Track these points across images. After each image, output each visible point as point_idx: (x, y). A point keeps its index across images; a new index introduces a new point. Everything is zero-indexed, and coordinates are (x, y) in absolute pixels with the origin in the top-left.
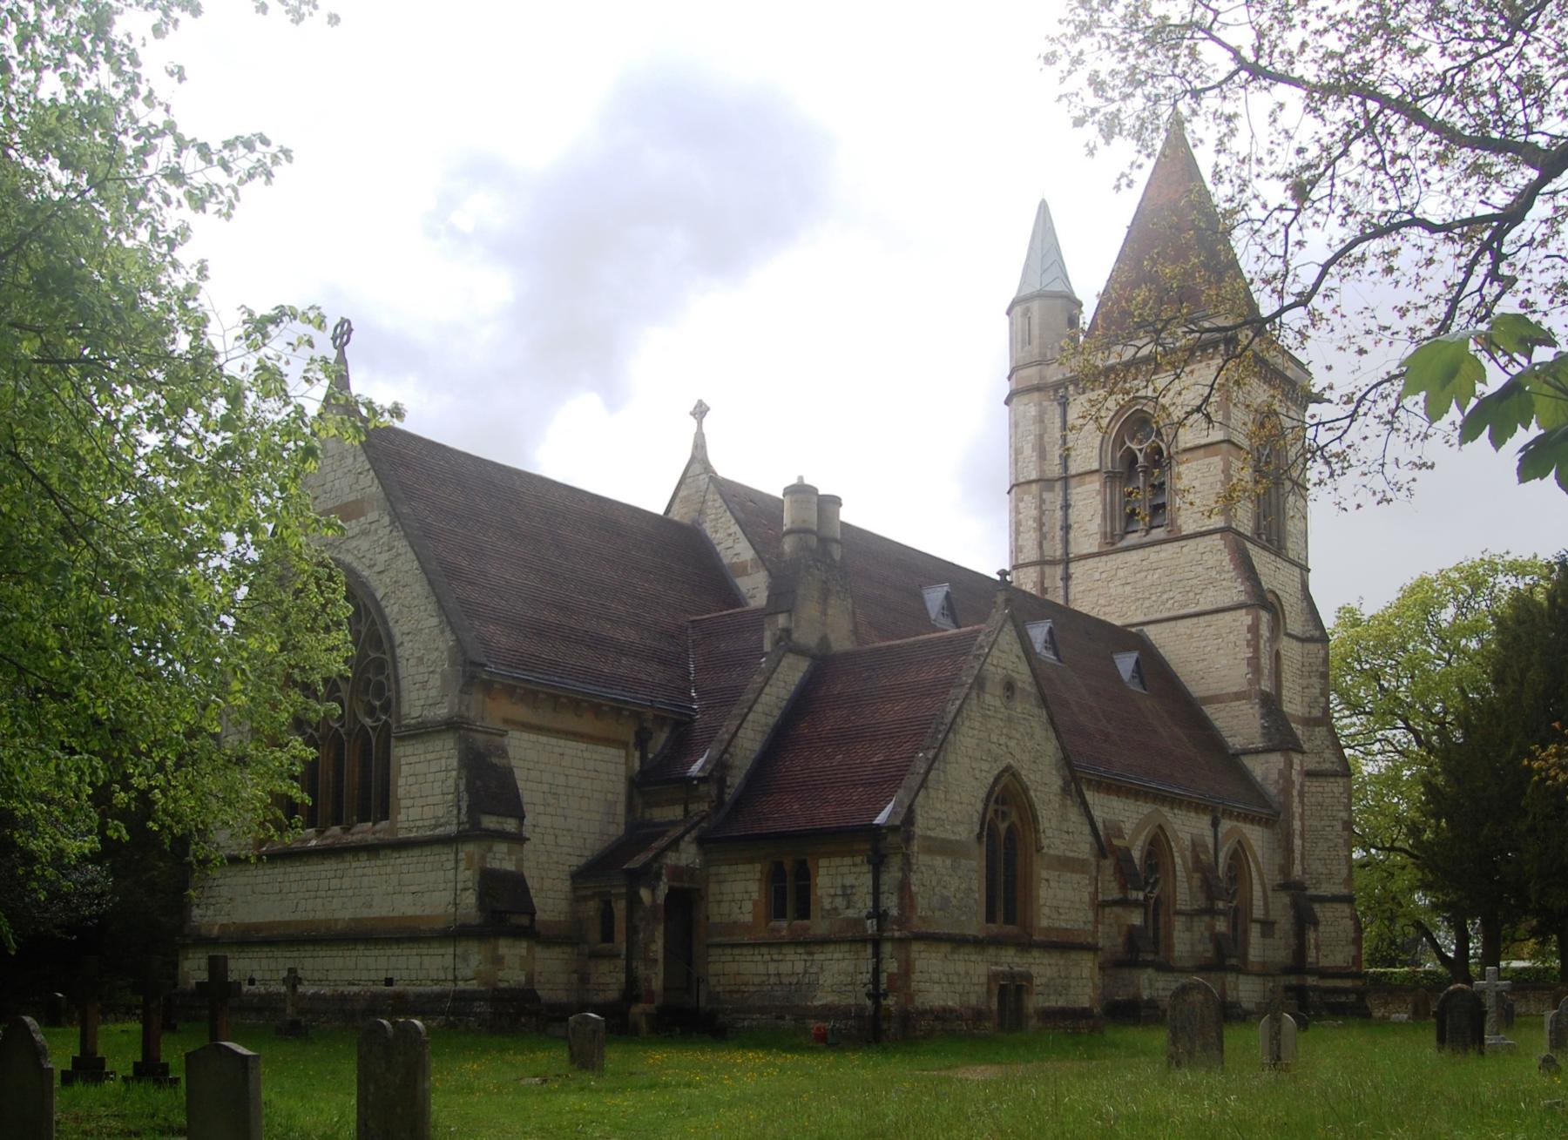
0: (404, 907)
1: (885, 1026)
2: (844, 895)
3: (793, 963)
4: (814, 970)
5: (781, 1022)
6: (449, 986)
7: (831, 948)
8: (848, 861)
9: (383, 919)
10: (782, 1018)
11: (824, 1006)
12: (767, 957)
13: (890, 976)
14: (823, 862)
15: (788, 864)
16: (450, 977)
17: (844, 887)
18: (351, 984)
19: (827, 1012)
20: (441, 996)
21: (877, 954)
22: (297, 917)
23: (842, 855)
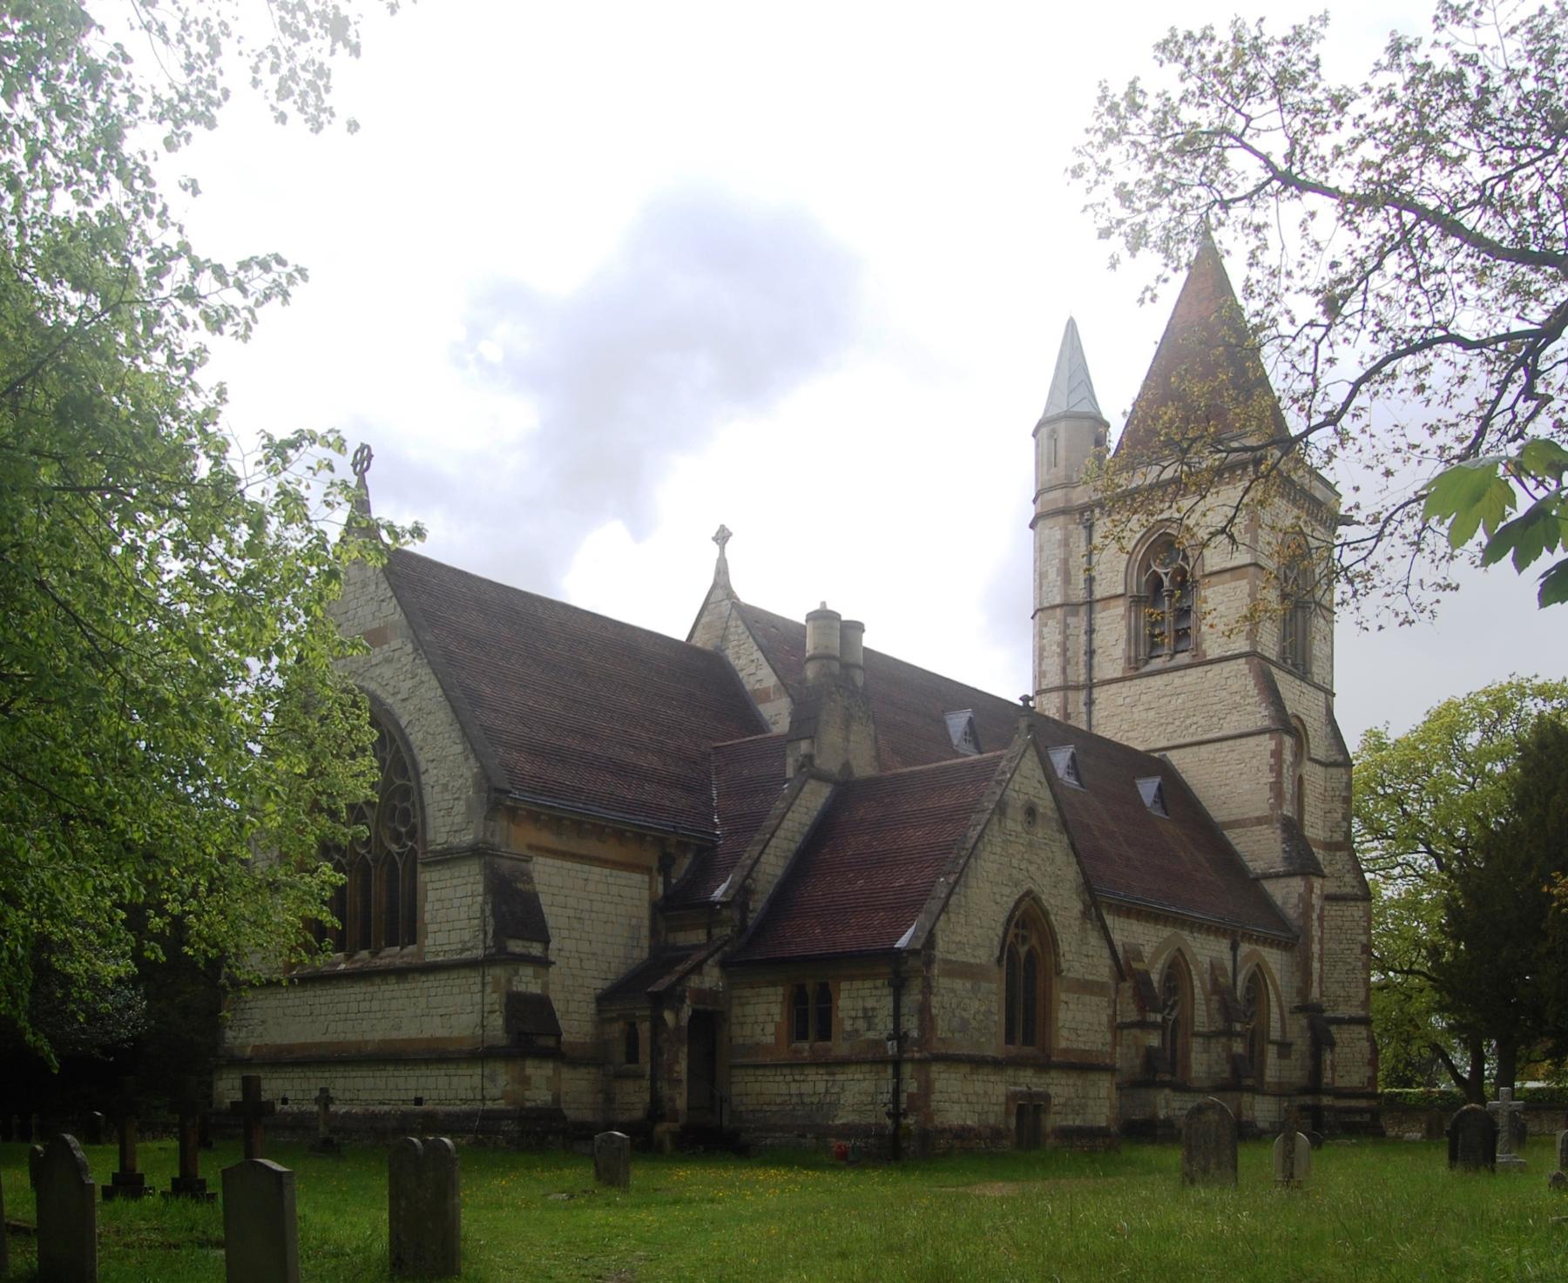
2: (865, 1017)
3: (814, 1083)
6: (478, 1106)
7: (853, 1068)
10: (804, 1136)
12: (789, 1078)
13: (910, 1096)
14: (844, 985)
17: (865, 1009)
19: (848, 1131)
20: (469, 1116)
21: (897, 1075)
23: (864, 977)
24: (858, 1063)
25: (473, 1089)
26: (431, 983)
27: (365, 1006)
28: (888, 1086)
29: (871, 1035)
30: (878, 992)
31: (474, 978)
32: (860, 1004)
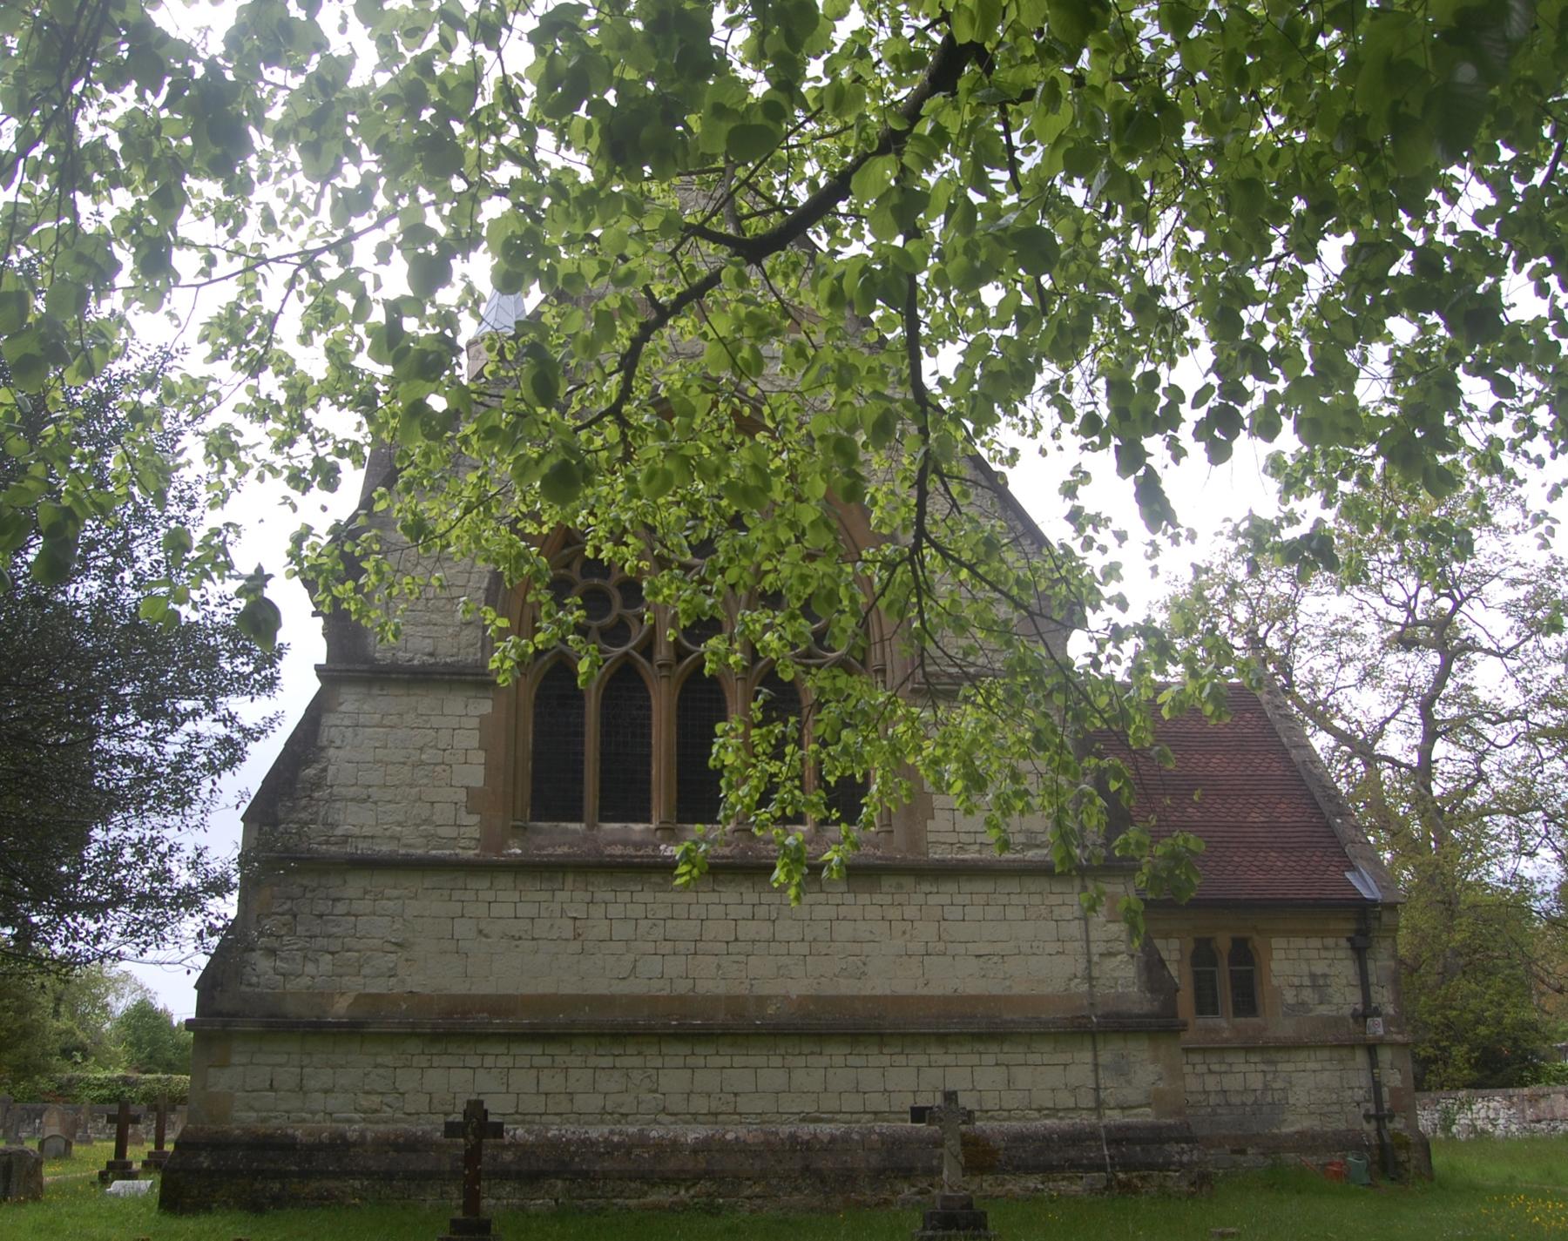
0: (956, 978)
1: (1402, 1156)
2: (1314, 986)
3: (1244, 1076)
4: (1278, 1085)
5: (1240, 1158)
6: (1086, 1120)
7: (1303, 1055)
8: (1315, 942)
9: (898, 1000)
10: (1243, 1152)
11: (1301, 1133)
12: (1201, 1068)
13: (1394, 1091)
14: (1277, 943)
15: (1223, 943)
16: (1088, 1101)
17: (1313, 976)
18: (806, 1119)
19: (1307, 1142)
20: (1074, 1138)
21: (1374, 1063)
22: (636, 987)
23: (1307, 934)
24: (1322, 1046)
25: (1074, 1090)
26: (943, 895)
27: (748, 929)
28: (1359, 1080)
29: (1323, 1010)
30: (1330, 954)
31: (1069, 900)
32: (1304, 968)
